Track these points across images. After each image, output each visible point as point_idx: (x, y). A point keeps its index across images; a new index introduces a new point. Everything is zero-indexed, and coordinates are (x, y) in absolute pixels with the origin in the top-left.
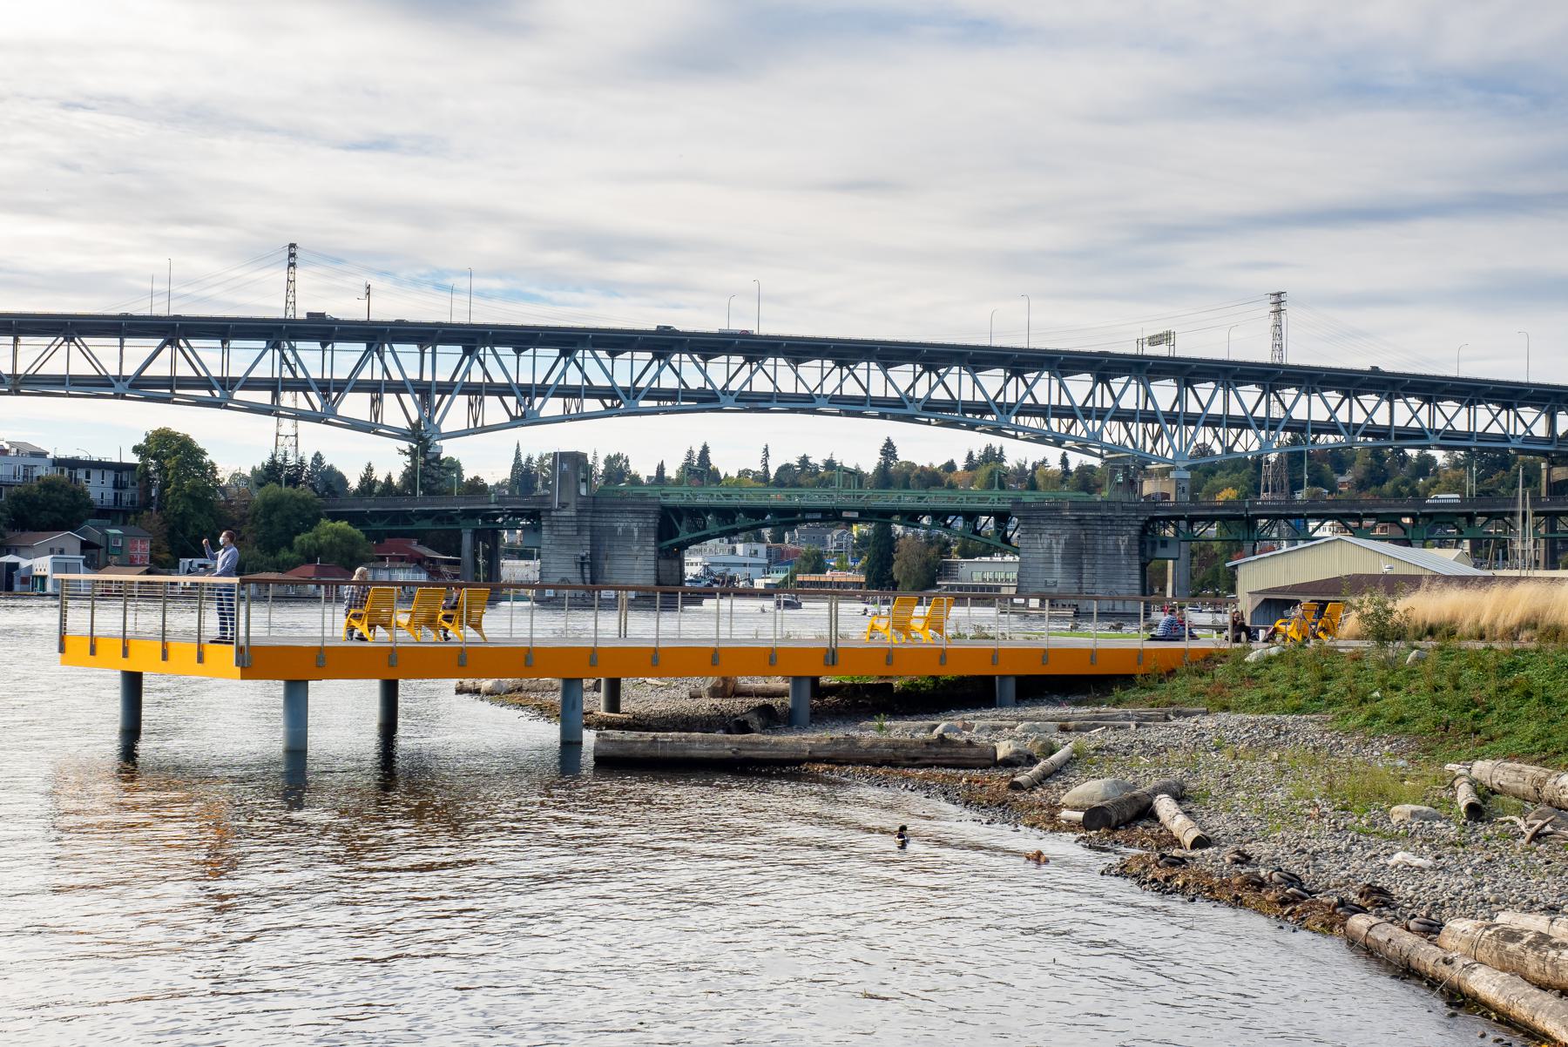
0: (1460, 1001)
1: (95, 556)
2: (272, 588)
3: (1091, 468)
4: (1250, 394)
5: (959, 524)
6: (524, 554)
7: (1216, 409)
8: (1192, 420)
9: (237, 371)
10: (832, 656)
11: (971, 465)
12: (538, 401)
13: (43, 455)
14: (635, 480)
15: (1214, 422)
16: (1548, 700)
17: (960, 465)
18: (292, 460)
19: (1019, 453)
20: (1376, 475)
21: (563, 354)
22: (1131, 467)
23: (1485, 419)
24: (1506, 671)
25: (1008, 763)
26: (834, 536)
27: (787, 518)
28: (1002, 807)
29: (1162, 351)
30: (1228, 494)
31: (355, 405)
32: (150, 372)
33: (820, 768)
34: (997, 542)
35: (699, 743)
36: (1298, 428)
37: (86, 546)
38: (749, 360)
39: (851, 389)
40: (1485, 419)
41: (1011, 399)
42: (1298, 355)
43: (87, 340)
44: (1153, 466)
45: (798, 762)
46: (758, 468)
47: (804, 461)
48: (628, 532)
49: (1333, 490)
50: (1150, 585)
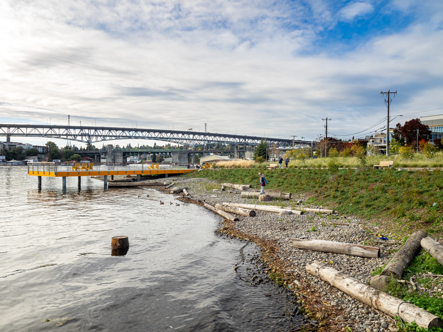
0: (216, 214)
1: (40, 159)
2: (68, 164)
3: (182, 146)
4: (202, 136)
5: (164, 153)
6: (104, 158)
7: (198, 138)
8: (195, 140)
9: (61, 133)
10: (142, 172)
11: (166, 146)
12: (106, 137)
13: (31, 145)
14: (120, 148)
15: (198, 140)
16: (234, 175)
17: (165, 146)
18: (70, 146)
19: (172, 144)
20: (218, 147)
21: (109, 131)
22: (187, 146)
23: (232, 140)
24: (229, 172)
25: (165, 185)
26: (148, 156)
27: (141, 153)
28: (163, 191)
29: (191, 131)
30: (200, 149)
31: (79, 138)
32: (48, 133)
33: (140, 187)
34: (169, 156)
35: (123, 184)
36: (208, 141)
37: (38, 158)
38: (136, 132)
39: (150, 136)
40: (232, 140)
41: (171, 137)
42: (72, 124)
43: (38, 129)
44: (190, 146)
45: (137, 186)
46: (137, 146)
47: (144, 146)
48: (119, 155)
49: (213, 149)
50: (190, 161)
